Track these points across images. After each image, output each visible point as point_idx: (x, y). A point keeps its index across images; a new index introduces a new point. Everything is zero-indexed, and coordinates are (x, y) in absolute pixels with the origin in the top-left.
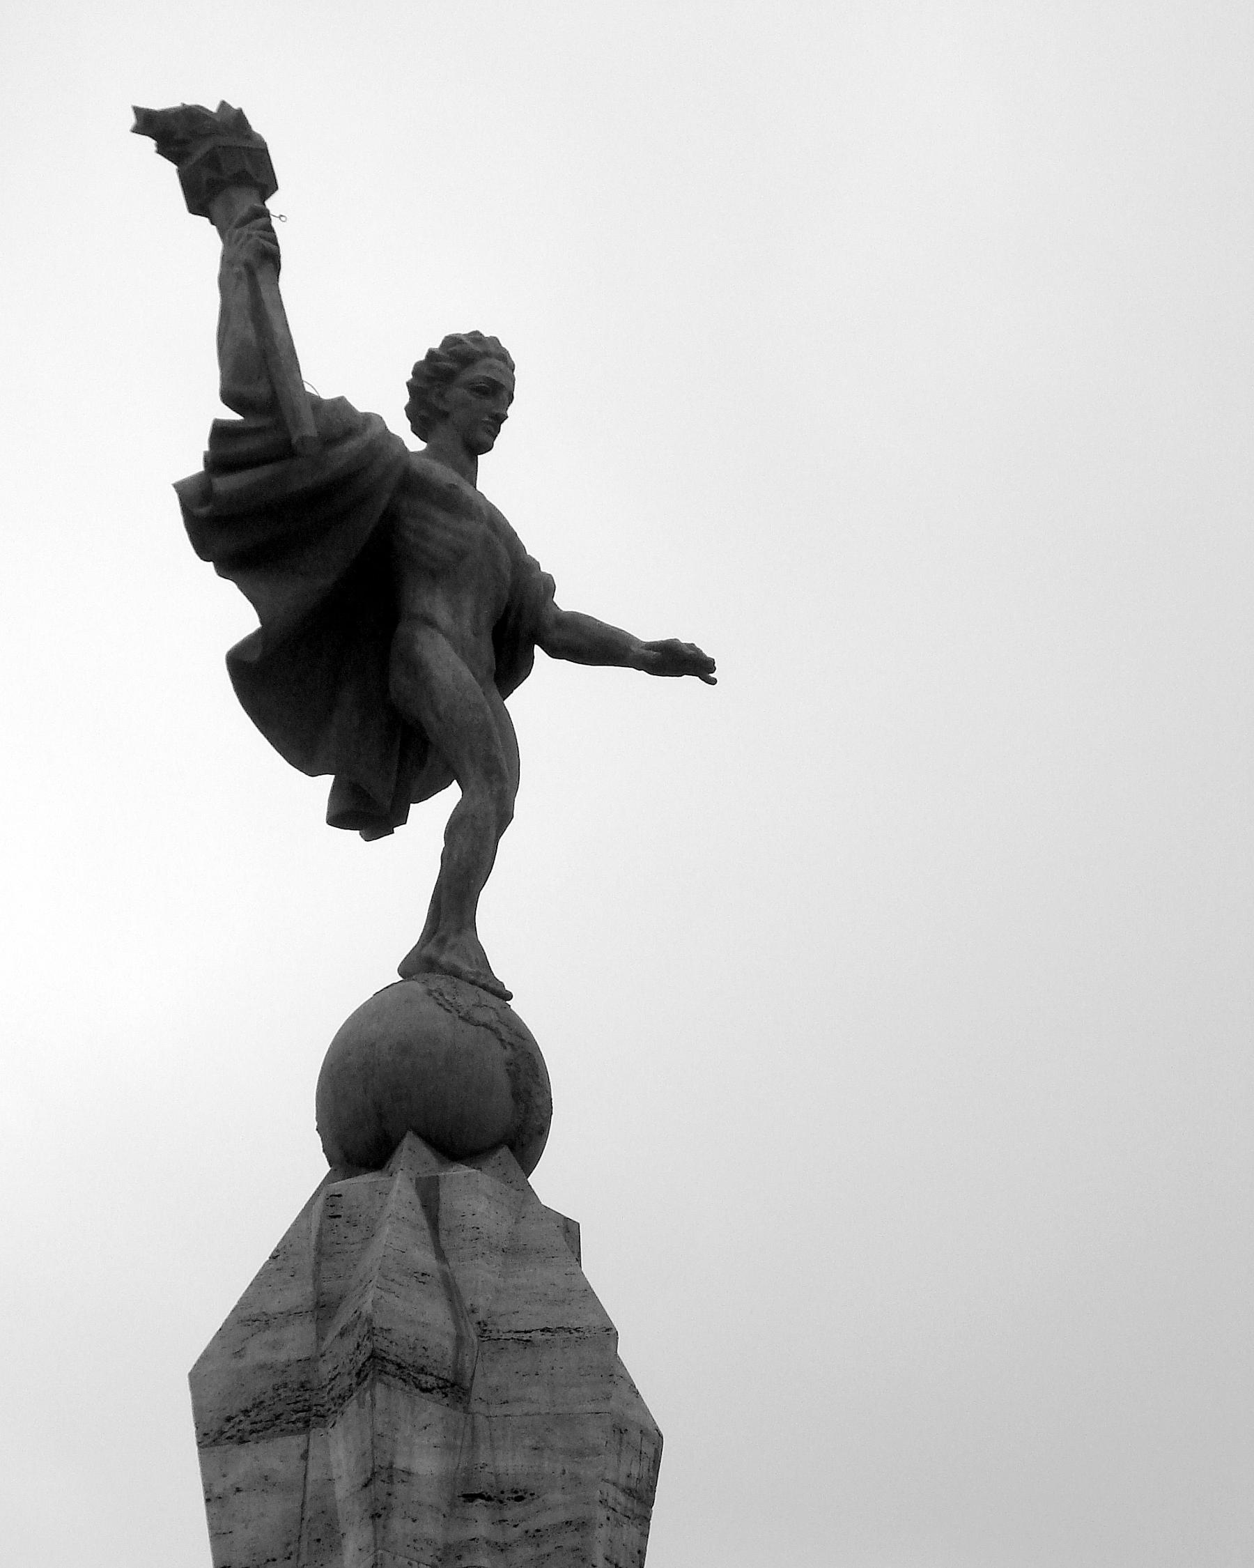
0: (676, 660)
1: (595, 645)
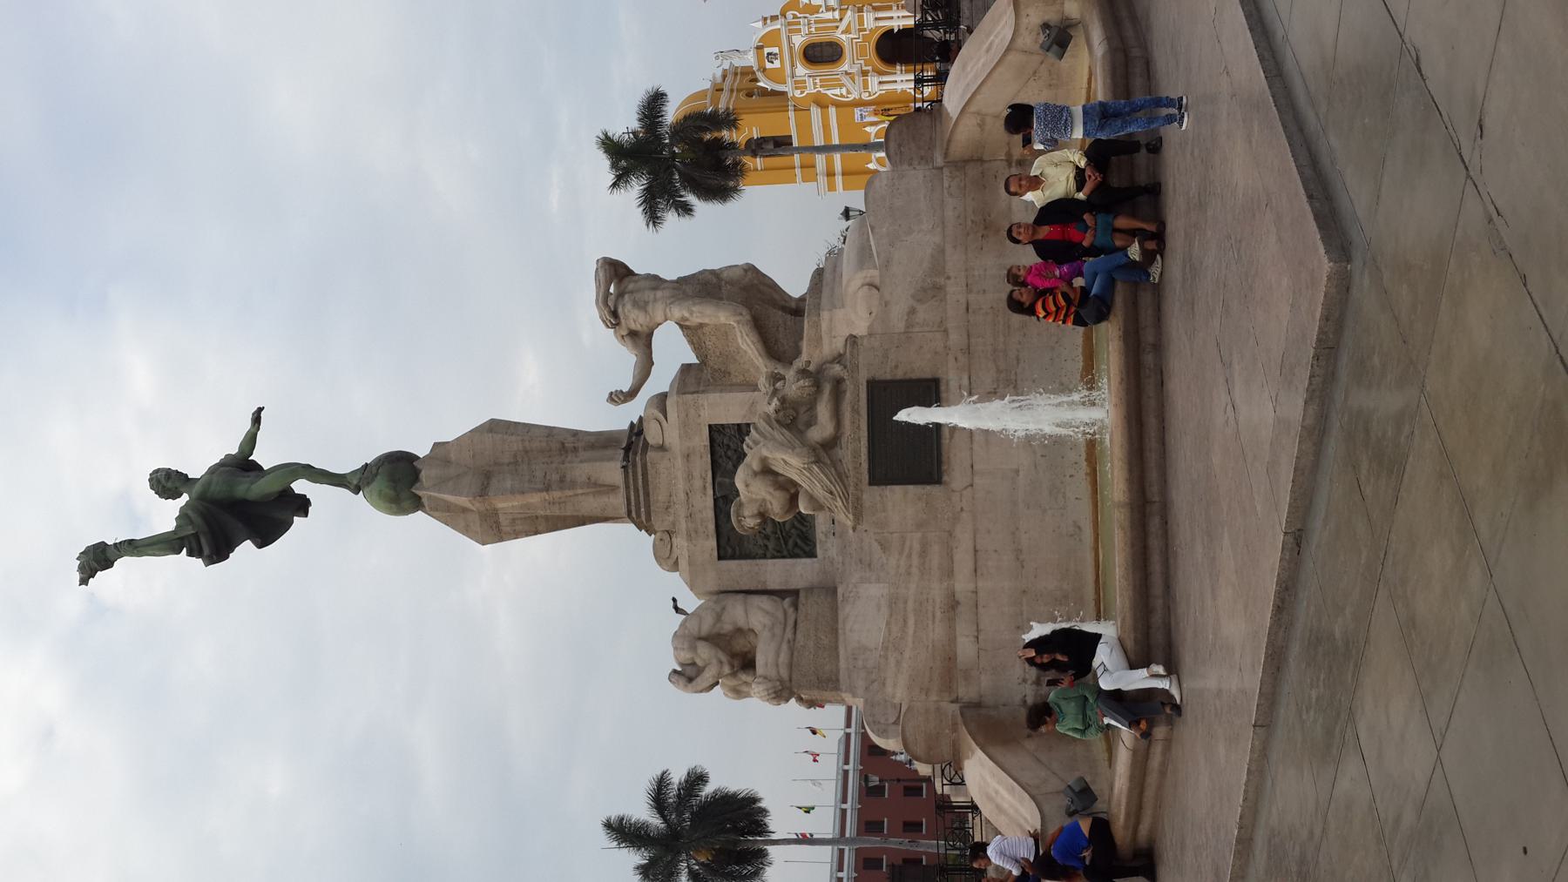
0: (257, 419)
1: (250, 441)
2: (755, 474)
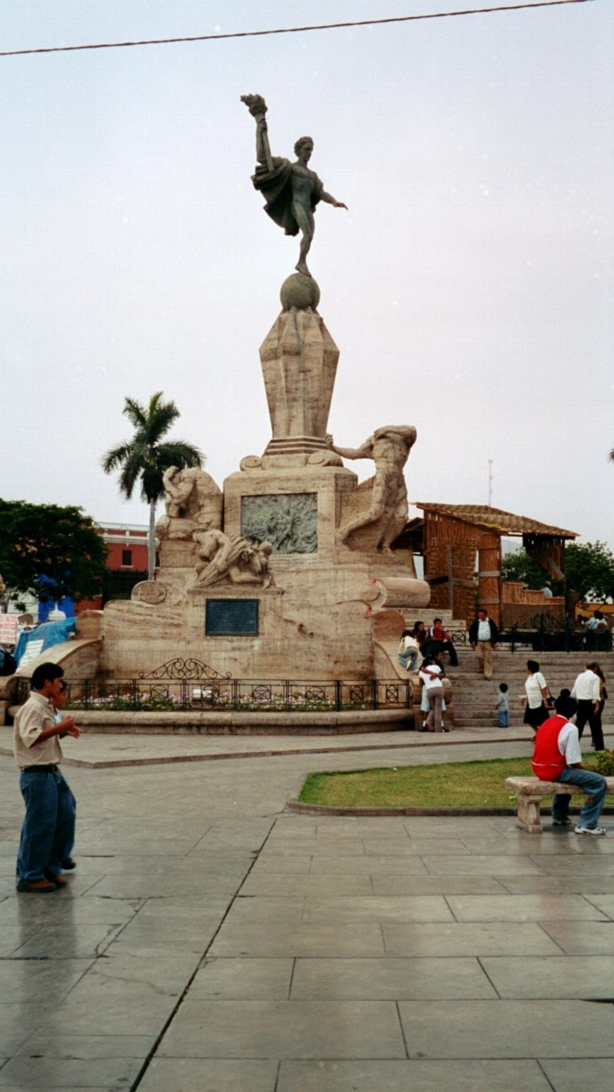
1: (329, 200)
2: (217, 540)
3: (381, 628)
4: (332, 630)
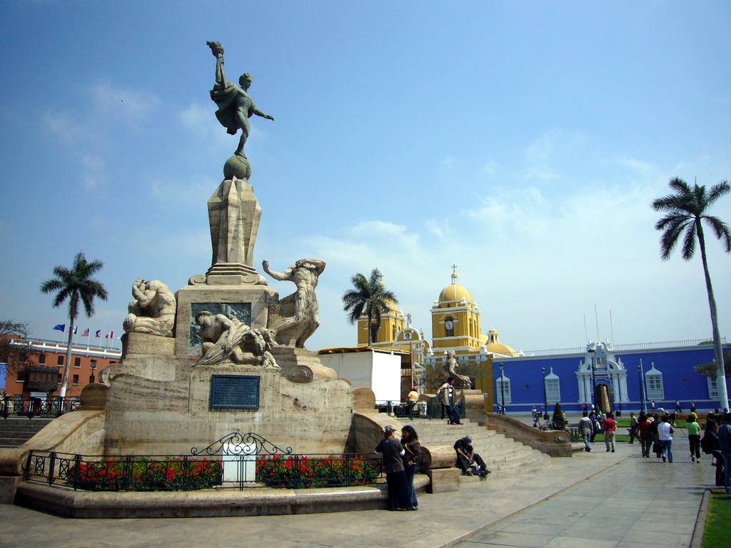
0: (269, 117)
3: (358, 402)
4: (321, 404)
